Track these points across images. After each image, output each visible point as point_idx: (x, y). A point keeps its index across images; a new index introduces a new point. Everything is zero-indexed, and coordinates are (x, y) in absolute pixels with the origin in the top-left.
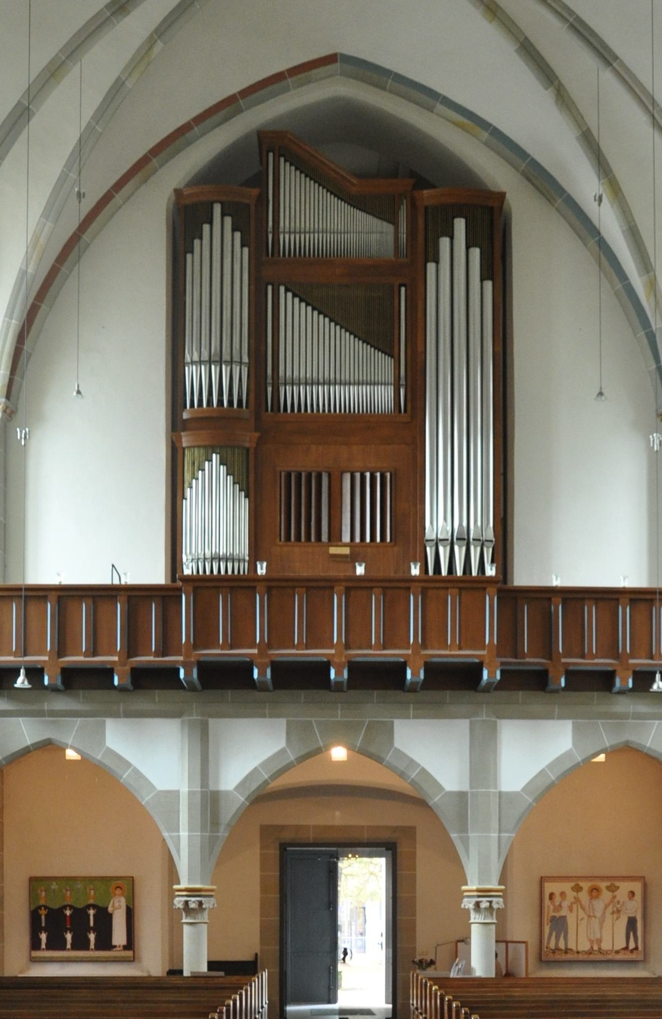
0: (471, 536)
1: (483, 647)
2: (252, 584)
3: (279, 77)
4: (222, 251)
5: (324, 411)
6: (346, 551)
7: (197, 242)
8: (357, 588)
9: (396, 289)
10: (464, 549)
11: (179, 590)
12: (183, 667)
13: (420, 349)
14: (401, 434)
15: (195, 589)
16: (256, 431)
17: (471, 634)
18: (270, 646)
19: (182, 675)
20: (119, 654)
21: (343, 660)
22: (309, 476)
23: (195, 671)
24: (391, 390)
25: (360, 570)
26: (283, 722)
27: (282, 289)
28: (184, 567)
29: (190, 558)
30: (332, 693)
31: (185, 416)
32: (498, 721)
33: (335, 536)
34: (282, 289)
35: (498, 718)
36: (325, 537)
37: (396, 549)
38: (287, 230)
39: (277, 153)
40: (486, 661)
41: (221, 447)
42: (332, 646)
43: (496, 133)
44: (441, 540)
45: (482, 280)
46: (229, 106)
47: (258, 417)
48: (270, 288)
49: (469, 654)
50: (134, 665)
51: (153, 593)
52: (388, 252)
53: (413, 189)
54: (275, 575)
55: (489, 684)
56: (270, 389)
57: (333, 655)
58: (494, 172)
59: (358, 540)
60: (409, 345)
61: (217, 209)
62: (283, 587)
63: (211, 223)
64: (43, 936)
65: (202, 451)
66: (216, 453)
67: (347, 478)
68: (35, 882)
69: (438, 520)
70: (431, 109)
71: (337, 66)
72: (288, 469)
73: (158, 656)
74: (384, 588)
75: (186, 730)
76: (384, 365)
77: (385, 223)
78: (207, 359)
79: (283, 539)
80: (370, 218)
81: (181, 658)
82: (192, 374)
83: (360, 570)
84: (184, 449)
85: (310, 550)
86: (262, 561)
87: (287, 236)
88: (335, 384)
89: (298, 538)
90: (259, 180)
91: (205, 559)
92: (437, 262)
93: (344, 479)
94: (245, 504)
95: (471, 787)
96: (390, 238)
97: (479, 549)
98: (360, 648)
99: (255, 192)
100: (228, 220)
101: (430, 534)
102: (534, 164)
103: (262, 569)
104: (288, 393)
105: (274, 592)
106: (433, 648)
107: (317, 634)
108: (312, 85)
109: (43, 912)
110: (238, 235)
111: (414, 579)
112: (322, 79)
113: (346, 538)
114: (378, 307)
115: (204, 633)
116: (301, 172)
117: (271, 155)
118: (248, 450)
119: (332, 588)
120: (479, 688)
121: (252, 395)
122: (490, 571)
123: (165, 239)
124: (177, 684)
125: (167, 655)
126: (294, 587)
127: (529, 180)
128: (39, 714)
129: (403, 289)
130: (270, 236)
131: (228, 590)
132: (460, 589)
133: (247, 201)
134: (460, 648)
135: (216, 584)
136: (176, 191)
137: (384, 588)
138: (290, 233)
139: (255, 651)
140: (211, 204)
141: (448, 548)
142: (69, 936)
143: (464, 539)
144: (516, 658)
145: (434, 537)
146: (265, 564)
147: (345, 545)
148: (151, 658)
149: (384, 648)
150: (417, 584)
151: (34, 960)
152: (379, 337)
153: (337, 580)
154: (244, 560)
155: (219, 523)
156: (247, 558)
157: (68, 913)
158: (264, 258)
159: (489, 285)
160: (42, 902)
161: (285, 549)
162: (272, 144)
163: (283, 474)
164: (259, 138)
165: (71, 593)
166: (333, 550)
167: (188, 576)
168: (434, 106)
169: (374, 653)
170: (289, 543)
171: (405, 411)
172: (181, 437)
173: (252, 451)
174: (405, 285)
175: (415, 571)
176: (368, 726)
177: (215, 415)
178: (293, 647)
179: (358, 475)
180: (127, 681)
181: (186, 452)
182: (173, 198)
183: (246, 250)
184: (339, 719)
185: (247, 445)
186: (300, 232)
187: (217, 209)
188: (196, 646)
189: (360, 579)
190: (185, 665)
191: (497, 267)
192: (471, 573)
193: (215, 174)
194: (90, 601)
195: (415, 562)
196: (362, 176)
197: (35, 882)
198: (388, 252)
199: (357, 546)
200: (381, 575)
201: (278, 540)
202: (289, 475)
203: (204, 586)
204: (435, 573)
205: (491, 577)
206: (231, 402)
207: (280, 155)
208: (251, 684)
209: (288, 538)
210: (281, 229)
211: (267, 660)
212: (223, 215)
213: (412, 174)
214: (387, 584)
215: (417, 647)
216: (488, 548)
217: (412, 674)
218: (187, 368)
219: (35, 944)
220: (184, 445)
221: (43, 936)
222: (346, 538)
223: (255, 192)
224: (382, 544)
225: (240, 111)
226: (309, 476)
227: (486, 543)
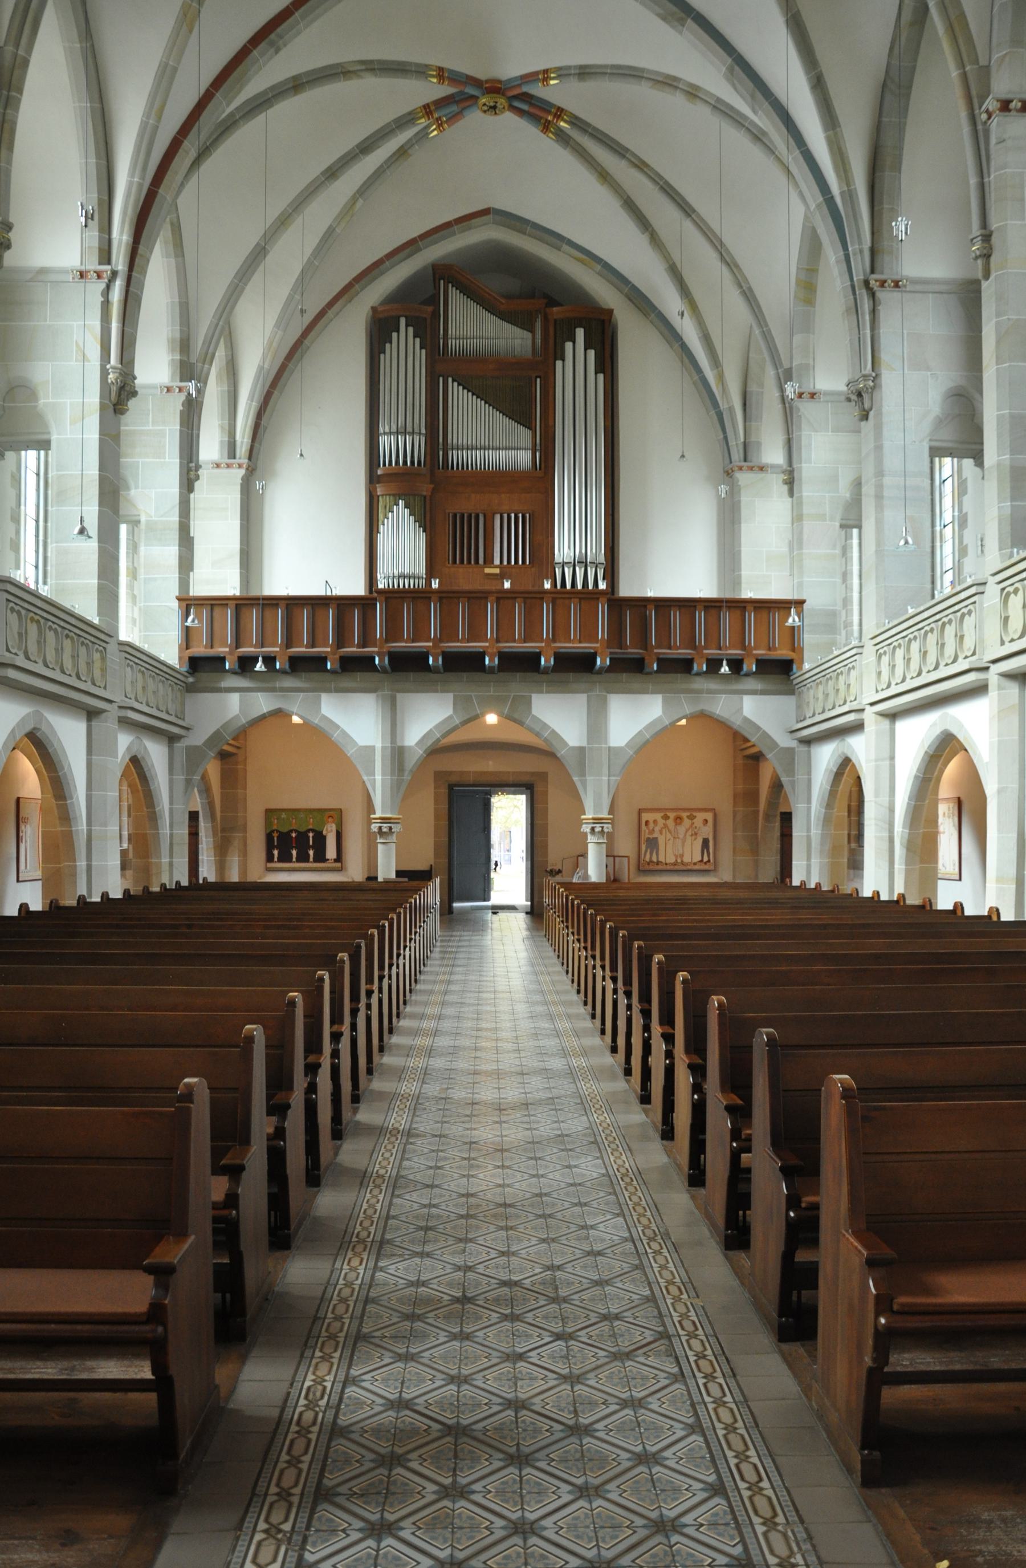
1: (597, 641)
3: (447, 225)
4: (406, 351)
6: (497, 571)
7: (388, 345)
11: (375, 599)
13: (551, 423)
15: (387, 599)
17: (588, 632)
18: (441, 640)
20: (331, 646)
22: (470, 516)
24: (529, 453)
26: (451, 696)
31: (379, 472)
33: (489, 561)
36: (481, 561)
40: (599, 651)
41: (405, 495)
42: (486, 640)
43: (607, 266)
46: (411, 246)
48: (441, 379)
49: (587, 647)
54: (445, 588)
55: (601, 668)
56: (441, 453)
59: (505, 563)
61: (403, 321)
63: (398, 331)
64: (276, 852)
67: (498, 517)
68: (269, 812)
69: (564, 549)
70: (559, 249)
76: (524, 435)
81: (376, 649)
86: (435, 578)
89: (462, 562)
90: (433, 300)
94: (423, 536)
95: (588, 743)
96: (529, 342)
98: (507, 642)
100: (411, 330)
101: (558, 558)
102: (634, 288)
104: (454, 456)
105: (444, 601)
106: (560, 642)
107: (475, 632)
109: (275, 835)
110: (418, 340)
111: (547, 592)
113: (497, 562)
114: (520, 392)
115: (393, 631)
117: (442, 282)
118: (425, 497)
119: (486, 598)
121: (428, 457)
127: (631, 300)
128: (273, 690)
129: (538, 380)
130: (441, 341)
132: (580, 599)
134: (580, 642)
137: (525, 598)
139: (431, 644)
142: (294, 852)
148: (354, 649)
149: (525, 642)
151: (269, 870)
155: (404, 550)
157: (294, 835)
159: (601, 376)
160: (275, 827)
162: (443, 274)
166: (487, 570)
173: (428, 498)
178: (458, 641)
179: (505, 516)
180: (337, 666)
183: (424, 351)
185: (425, 493)
187: (403, 321)
188: (387, 641)
189: (507, 591)
190: (379, 654)
191: (607, 364)
194: (310, 608)
195: (547, 579)
196: (509, 297)
197: (269, 812)
199: (505, 567)
200: (522, 588)
202: (455, 516)
206: (412, 462)
208: (427, 668)
209: (454, 562)
211: (439, 651)
212: (407, 326)
213: (545, 296)
215: (437, 641)
219: (270, 858)
221: (276, 852)
222: (497, 562)
223: (430, 309)
225: (419, 250)
226: (470, 516)
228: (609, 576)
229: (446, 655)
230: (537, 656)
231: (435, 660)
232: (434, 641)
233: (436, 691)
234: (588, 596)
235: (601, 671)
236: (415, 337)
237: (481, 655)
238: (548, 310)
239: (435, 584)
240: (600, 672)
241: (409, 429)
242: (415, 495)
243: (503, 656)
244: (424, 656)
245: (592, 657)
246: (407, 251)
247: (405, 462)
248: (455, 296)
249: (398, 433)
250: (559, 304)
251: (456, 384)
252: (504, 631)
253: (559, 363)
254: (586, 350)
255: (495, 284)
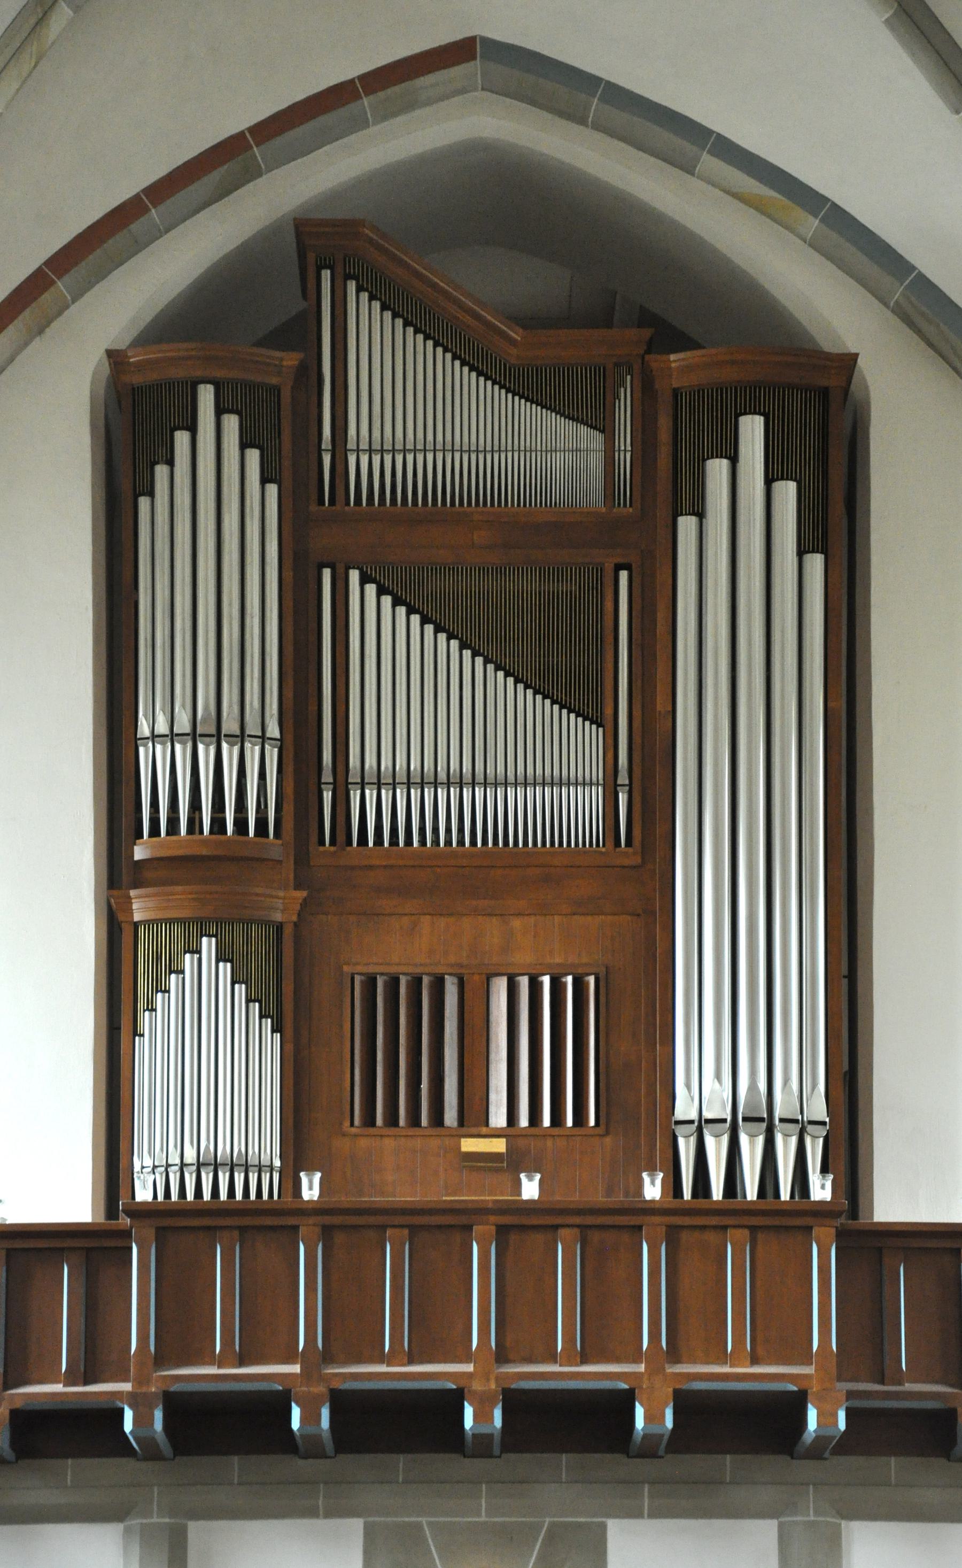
0: (777, 1114)
1: (805, 1356)
2: (291, 1221)
3: (338, 96)
4: (216, 478)
5: (448, 842)
6: (499, 1146)
7: (161, 471)
8: (523, 1228)
9: (609, 580)
10: (760, 1140)
11: (126, 1234)
12: (131, 1406)
13: (661, 704)
14: (632, 866)
15: (161, 1234)
16: (298, 887)
17: (779, 1330)
18: (328, 1357)
19: (128, 1426)
21: (493, 1386)
22: (416, 983)
23: (158, 1415)
24: (597, 794)
25: (530, 1189)
26: (356, 1525)
27: (354, 576)
28: (137, 1183)
29: (148, 1162)
30: (467, 1460)
31: (139, 853)
32: (844, 1523)
33: (473, 1115)
34: (354, 576)
35: (844, 1517)
36: (450, 1116)
37: (608, 1140)
38: (364, 445)
39: (339, 269)
40: (815, 1388)
41: (219, 922)
42: (466, 1356)
43: (838, 219)
44: (708, 1121)
45: (801, 553)
46: (227, 162)
47: (302, 859)
48: (327, 574)
49: (775, 1374)
50: (18, 1404)
51: (68, 1243)
52: (590, 491)
53: (649, 351)
54: (344, 1199)
55: (820, 1439)
56: (327, 796)
57: (470, 1375)
58: (831, 308)
59: (524, 1122)
60: (638, 684)
61: (206, 396)
62: (355, 1227)
63: (192, 429)
65: (177, 930)
66: (209, 936)
67: (500, 987)
69: (701, 1086)
70: (689, 168)
71: (471, 69)
72: (371, 969)
73: (74, 1384)
74: (583, 1228)
75: (136, 1549)
76: (581, 743)
77: (584, 429)
78: (187, 729)
79: (357, 1121)
80: (552, 420)
81: (127, 1387)
82: (154, 761)
83: (530, 1189)
84: (136, 925)
85: (418, 1143)
86: (310, 1170)
87: (364, 459)
88: (473, 784)
89: (392, 1119)
90: (299, 332)
91: (183, 1165)
92: (700, 514)
93: (493, 989)
94: (272, 1044)
96: (596, 462)
97: (794, 1140)
98: (530, 1360)
99: (291, 360)
100: (232, 423)
101: (684, 1108)
102: (924, 285)
103: (311, 1188)
104: (366, 804)
105: (339, 1238)
106: (694, 1361)
107: (433, 1331)
108: (417, 113)
110: (254, 456)
111: (650, 1209)
112: (442, 98)
113: (498, 1118)
114: (569, 612)
115: (180, 1332)
116: (395, 316)
117: (326, 274)
118: (280, 927)
119: (468, 1228)
120: (799, 1449)
121: (289, 808)
122: (821, 1189)
123: (88, 455)
124: (118, 1445)
125: (95, 1381)
126: (383, 1228)
127: (911, 324)
129: (624, 575)
130: (327, 459)
131: (236, 1233)
132: (753, 1229)
133: (274, 381)
134: (755, 1361)
135: (207, 1222)
136: (110, 353)
137: (583, 1228)
138: (370, 451)
139: (296, 1369)
140: (193, 386)
141: (725, 1139)
143: (761, 1120)
144: (882, 1382)
145: (694, 1115)
146: (318, 1175)
147: (497, 1134)
148: (58, 1388)
149: (584, 1360)
150: (657, 1219)
152: (572, 685)
153: (480, 1211)
154: (271, 1168)
155: (218, 1092)
156: (277, 1163)
158: (314, 508)
159: (816, 562)
161: (363, 1143)
162: (333, 248)
163: (358, 979)
164: (299, 234)
165: (31, 1244)
166: (469, 1145)
167: (144, 1203)
168: (697, 159)
169: (561, 1371)
170: (372, 1131)
171: (629, 843)
172: (129, 900)
173: (288, 931)
174: (628, 567)
175: (653, 1190)
176: (549, 1530)
177: (205, 852)
178: (381, 1358)
179: (524, 982)
181: (141, 930)
182: (106, 370)
183: (272, 489)
184: (483, 1519)
185: (278, 917)
186: (394, 451)
187: (206, 396)
188: (161, 1360)
189: (530, 1208)
190: (134, 1400)
191: (836, 525)
192: (777, 1195)
193: (196, 318)
195: (652, 1170)
196: (529, 322)
198: (590, 491)
199: (523, 1134)
200: (575, 1198)
201: (347, 1123)
202: (371, 982)
203: (182, 1226)
204: (695, 1195)
205: (822, 1203)
206: (241, 824)
207: (348, 277)
208: (286, 1443)
209: (369, 1120)
210: (351, 445)
211: (321, 1389)
212: (220, 411)
213: (646, 318)
214: (590, 1220)
215: (656, 1359)
216: (814, 1137)
217: (647, 1418)
218: (142, 750)
220: (137, 917)
222: (498, 1118)
223: (291, 360)
224: (579, 1131)
225: (252, 173)
226: (416, 983)
227: (810, 1128)
228: (842, 1163)
229: (345, 1404)
230: (623, 1403)
231: (310, 1417)
232: (305, 1359)
233: (311, 1512)
234: (778, 1222)
235: (821, 1449)
236: (244, 446)
237: (452, 1401)
238: (655, 361)
239: (311, 1188)
240: (819, 1449)
241: (230, 725)
242: (249, 922)
243: (518, 1403)
244: (274, 1405)
245: (794, 1405)
246: (216, 176)
247: (218, 824)
248: (371, 332)
249: (194, 736)
250: (684, 342)
251: (371, 589)
252: (519, 1324)
253: (687, 525)
254: (769, 482)
255: (489, 281)
